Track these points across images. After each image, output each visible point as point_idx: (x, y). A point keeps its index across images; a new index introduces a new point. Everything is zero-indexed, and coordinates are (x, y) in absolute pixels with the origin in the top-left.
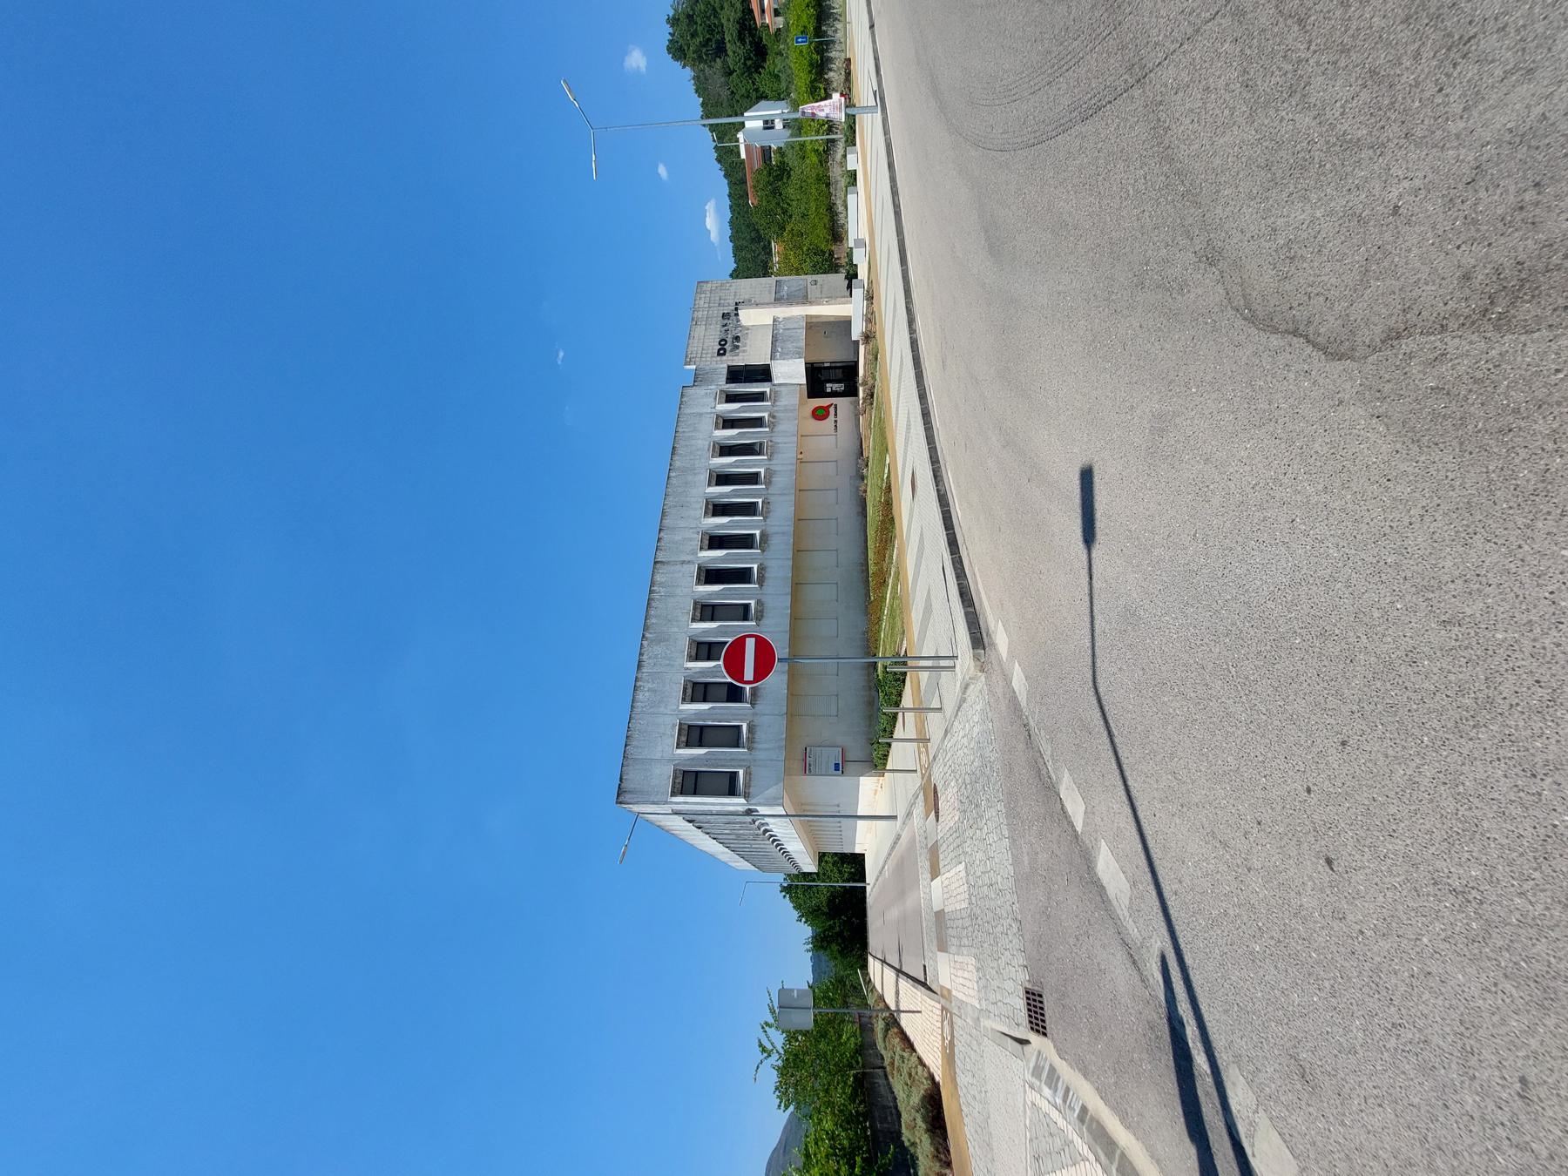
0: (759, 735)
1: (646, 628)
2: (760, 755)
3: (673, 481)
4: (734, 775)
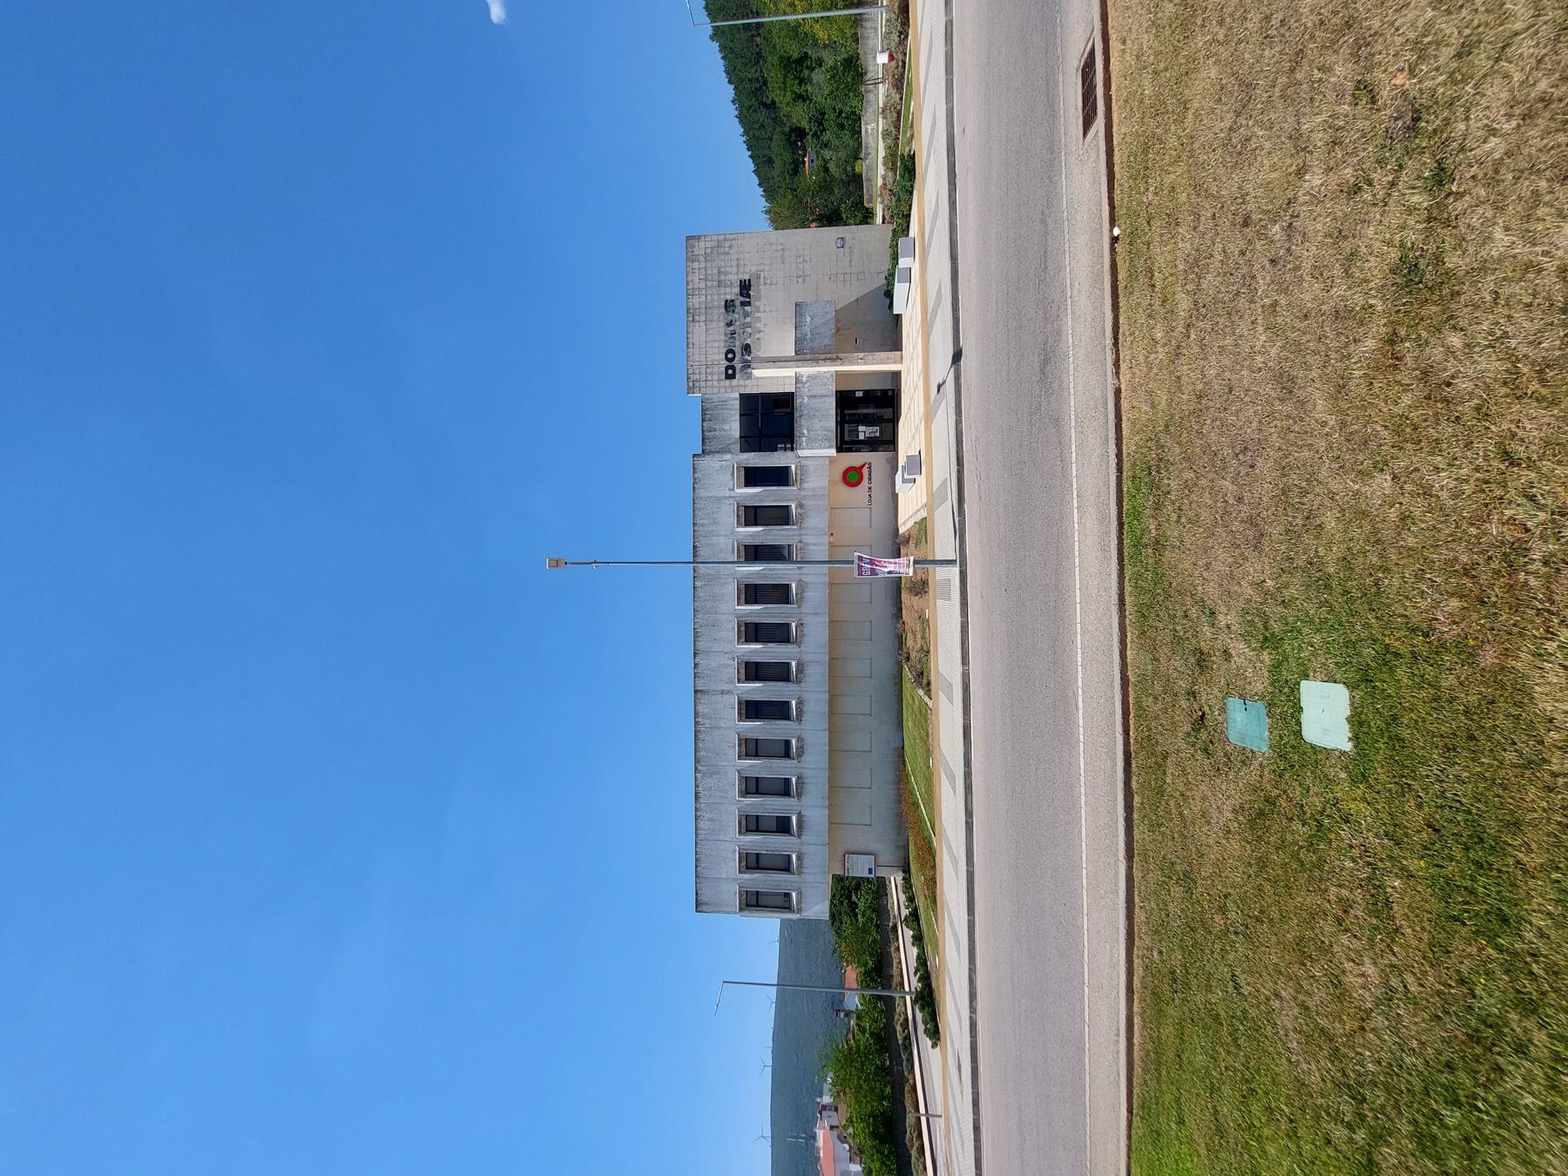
0: (806, 862)
1: (697, 761)
2: (809, 878)
3: (700, 593)
4: (788, 743)
